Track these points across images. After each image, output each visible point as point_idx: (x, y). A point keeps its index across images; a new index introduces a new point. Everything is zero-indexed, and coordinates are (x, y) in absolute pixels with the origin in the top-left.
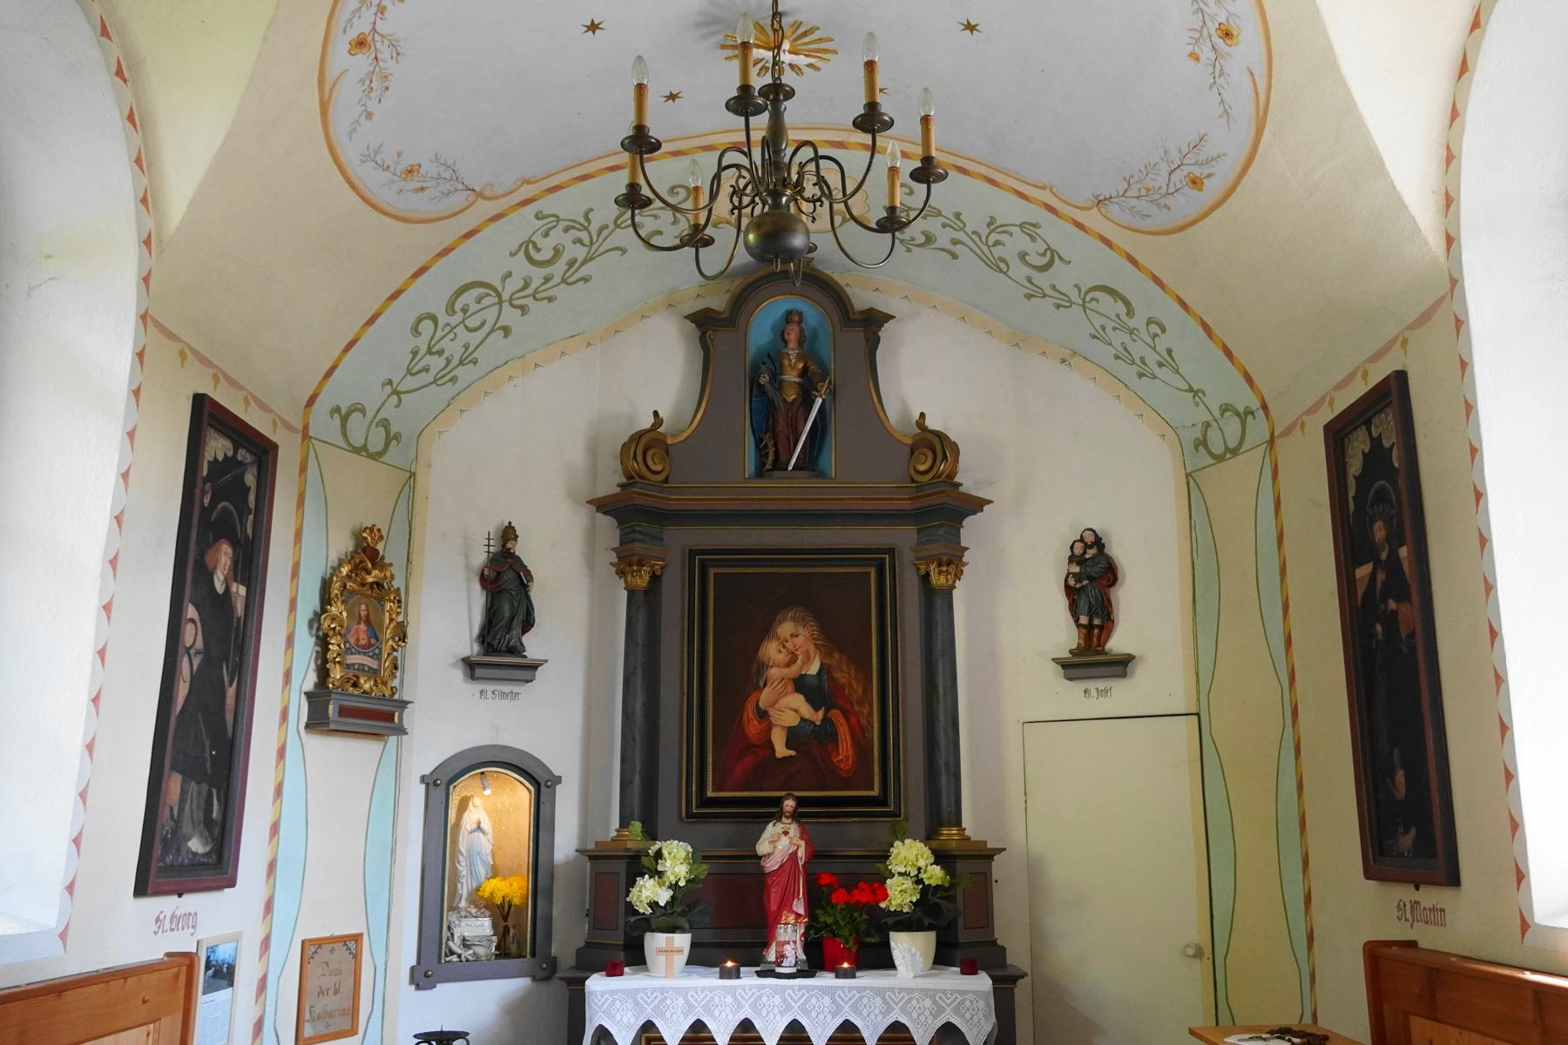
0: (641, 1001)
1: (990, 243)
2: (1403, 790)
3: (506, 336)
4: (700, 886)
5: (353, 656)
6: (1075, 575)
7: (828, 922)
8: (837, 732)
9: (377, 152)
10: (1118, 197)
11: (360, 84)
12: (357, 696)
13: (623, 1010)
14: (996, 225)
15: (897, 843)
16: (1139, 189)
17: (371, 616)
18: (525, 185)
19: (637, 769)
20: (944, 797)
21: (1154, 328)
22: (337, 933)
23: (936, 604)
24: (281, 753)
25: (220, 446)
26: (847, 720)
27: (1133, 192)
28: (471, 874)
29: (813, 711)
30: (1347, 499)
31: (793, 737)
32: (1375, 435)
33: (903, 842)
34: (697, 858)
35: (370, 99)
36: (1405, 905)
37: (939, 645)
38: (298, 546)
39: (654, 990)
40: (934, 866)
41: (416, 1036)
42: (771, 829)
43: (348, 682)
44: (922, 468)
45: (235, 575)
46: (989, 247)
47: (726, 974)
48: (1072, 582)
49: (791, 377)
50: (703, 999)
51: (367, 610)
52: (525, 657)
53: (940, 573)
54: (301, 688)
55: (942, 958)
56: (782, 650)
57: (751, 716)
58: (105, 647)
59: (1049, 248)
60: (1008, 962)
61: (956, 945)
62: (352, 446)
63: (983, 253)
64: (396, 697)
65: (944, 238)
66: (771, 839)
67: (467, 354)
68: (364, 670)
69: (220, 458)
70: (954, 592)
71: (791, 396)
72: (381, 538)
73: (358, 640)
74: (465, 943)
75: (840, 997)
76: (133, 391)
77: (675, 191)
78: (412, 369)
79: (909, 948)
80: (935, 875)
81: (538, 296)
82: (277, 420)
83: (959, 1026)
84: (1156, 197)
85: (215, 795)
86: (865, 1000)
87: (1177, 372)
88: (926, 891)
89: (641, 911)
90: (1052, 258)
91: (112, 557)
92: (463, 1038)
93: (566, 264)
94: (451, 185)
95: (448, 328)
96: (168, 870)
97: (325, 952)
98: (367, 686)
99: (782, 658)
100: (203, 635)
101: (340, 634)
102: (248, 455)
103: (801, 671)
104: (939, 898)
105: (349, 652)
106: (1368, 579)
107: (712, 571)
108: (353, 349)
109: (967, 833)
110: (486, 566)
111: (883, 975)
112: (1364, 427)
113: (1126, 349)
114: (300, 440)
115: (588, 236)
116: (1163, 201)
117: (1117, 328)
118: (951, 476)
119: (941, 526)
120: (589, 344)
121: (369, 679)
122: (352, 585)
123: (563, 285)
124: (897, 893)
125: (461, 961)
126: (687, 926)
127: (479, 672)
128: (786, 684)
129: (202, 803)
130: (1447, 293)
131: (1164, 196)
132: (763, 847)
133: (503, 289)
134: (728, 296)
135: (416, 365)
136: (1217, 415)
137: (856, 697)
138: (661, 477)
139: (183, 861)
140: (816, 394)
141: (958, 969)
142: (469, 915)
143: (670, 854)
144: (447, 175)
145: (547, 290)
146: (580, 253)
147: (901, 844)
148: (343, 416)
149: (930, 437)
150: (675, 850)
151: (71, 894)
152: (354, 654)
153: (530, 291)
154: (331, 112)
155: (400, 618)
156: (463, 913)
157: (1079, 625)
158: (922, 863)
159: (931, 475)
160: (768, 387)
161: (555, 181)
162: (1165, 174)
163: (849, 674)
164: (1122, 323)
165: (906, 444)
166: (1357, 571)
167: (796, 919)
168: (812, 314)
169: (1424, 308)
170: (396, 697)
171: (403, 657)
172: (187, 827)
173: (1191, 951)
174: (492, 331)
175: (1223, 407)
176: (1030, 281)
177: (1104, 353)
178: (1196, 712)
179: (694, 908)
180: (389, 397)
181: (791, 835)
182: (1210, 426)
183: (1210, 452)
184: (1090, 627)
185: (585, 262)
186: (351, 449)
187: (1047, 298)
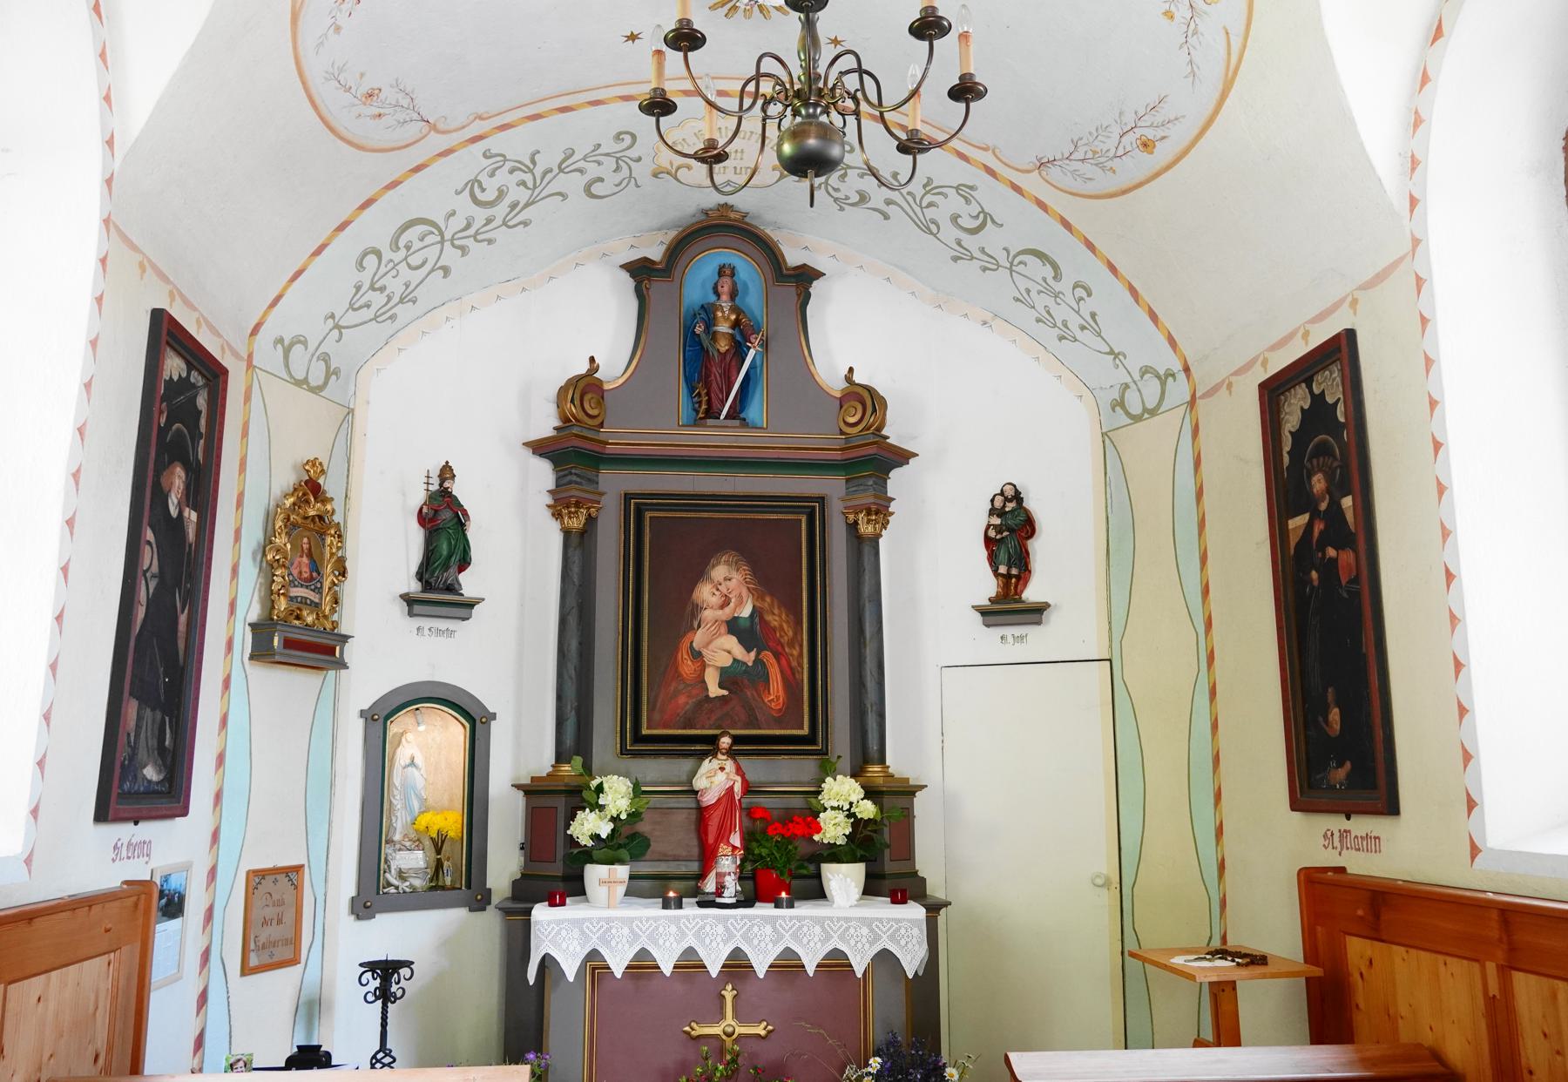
1: (924, 205)
2: (1337, 727)
3: (445, 277)
5: (295, 589)
7: (764, 854)
9: (341, 70)
12: (299, 628)
14: (932, 186)
16: (1086, 152)
17: (313, 549)
21: (1080, 292)
22: (280, 864)
23: (864, 550)
25: (175, 365)
27: (1079, 155)
30: (1282, 455)
31: (727, 678)
32: (1316, 391)
35: (340, 11)
36: (1332, 835)
37: (867, 589)
40: (865, 801)
41: (361, 965)
42: (708, 765)
44: (852, 420)
45: (188, 500)
46: (922, 208)
48: (992, 533)
49: (723, 328)
51: (310, 544)
52: (462, 595)
53: (869, 522)
55: (872, 888)
57: (685, 656)
58: (67, 563)
59: (983, 211)
62: (295, 379)
63: (915, 213)
64: (336, 631)
67: (407, 292)
68: (306, 603)
69: (175, 378)
70: (881, 540)
71: (723, 346)
72: (323, 471)
73: (300, 573)
74: (401, 875)
75: (781, 926)
76: (96, 298)
79: (844, 879)
80: (867, 810)
81: (479, 237)
85: (167, 723)
87: (1099, 335)
88: (858, 823)
89: (583, 843)
90: (985, 219)
91: (74, 470)
92: (409, 967)
93: (509, 207)
94: (407, 114)
95: (391, 265)
96: (125, 796)
97: (268, 883)
98: (310, 619)
99: (715, 600)
100: (159, 560)
101: (284, 566)
102: (200, 378)
104: (869, 831)
105: (292, 585)
106: (1302, 531)
107: (648, 515)
108: (299, 279)
109: (890, 770)
110: (425, 504)
111: (821, 905)
112: (1304, 385)
113: (1048, 312)
115: (531, 177)
116: (1109, 164)
121: (312, 612)
122: (295, 517)
126: (628, 858)
127: (417, 608)
128: (719, 626)
129: (156, 732)
130: (1407, 254)
131: (1111, 159)
133: (446, 228)
134: (664, 247)
135: (358, 300)
136: (1137, 377)
137: (786, 638)
138: (597, 422)
139: (139, 789)
140: (750, 345)
141: (889, 899)
144: (405, 102)
145: (487, 232)
146: (523, 195)
148: (286, 347)
149: (860, 390)
151: (35, 818)
152: (297, 586)
153: (471, 231)
154: (300, 23)
155: (340, 555)
156: (398, 846)
157: (996, 573)
158: (854, 798)
159: (860, 427)
160: (703, 336)
161: (507, 118)
163: (780, 617)
164: (1048, 287)
165: (835, 397)
166: (1290, 522)
167: (733, 851)
168: (748, 270)
169: (1379, 269)
170: (336, 631)
172: (142, 754)
173: (1099, 881)
174: (433, 270)
175: (1143, 370)
176: (959, 243)
177: (1026, 316)
180: (331, 330)
182: (1129, 388)
183: (1128, 413)
185: (527, 205)
186: (292, 381)
187: (975, 260)
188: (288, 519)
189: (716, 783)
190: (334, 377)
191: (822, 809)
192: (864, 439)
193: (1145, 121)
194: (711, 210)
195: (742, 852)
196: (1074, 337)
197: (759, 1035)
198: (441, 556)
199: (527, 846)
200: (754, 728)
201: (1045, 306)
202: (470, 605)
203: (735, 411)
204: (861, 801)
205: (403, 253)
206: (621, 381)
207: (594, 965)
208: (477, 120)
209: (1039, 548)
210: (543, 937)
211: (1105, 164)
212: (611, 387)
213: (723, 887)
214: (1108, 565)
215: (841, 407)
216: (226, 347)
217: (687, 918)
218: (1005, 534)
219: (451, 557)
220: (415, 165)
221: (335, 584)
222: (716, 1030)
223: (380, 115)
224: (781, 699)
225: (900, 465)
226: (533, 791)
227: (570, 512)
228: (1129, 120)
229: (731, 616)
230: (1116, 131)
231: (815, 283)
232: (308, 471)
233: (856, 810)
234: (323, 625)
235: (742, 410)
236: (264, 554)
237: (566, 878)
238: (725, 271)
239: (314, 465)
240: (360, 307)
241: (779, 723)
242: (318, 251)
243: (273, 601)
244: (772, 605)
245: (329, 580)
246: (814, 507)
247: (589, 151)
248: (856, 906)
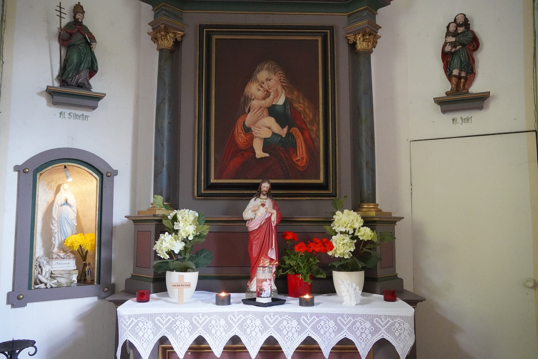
4: (204, 240)
6: (451, 43)
8: (296, 142)
15: (338, 213)
19: (165, 164)
20: (365, 184)
26: (303, 134)
28: (61, 231)
29: (280, 128)
31: (267, 145)
33: (342, 212)
34: (199, 221)
39: (167, 315)
40: (365, 228)
42: (254, 203)
47: (220, 302)
52: (91, 91)
57: (240, 131)
61: (375, 280)
66: (253, 209)
70: (372, 55)
74: (52, 276)
80: (366, 233)
83: (391, 341)
86: (322, 323)
88: (360, 244)
89: (162, 257)
92: (33, 346)
99: (260, 94)
103: (273, 103)
107: (214, 37)
109: (379, 207)
124: (340, 245)
125: (47, 288)
127: (57, 98)
128: (263, 111)
132: (247, 214)
137: (308, 119)
141: (382, 296)
142: (59, 257)
147: (341, 213)
150: (186, 216)
157: (449, 76)
158: (357, 225)
163: (304, 104)
167: (270, 262)
173: (531, 284)
178: (535, 130)
181: (267, 206)
191: (334, 233)
198: (72, 63)
200: (286, 179)
202: (98, 98)
210: (125, 328)
213: (262, 290)
218: (458, 47)
219: (81, 64)
224: (305, 159)
229: (271, 104)
233: (358, 234)
246: (327, 32)
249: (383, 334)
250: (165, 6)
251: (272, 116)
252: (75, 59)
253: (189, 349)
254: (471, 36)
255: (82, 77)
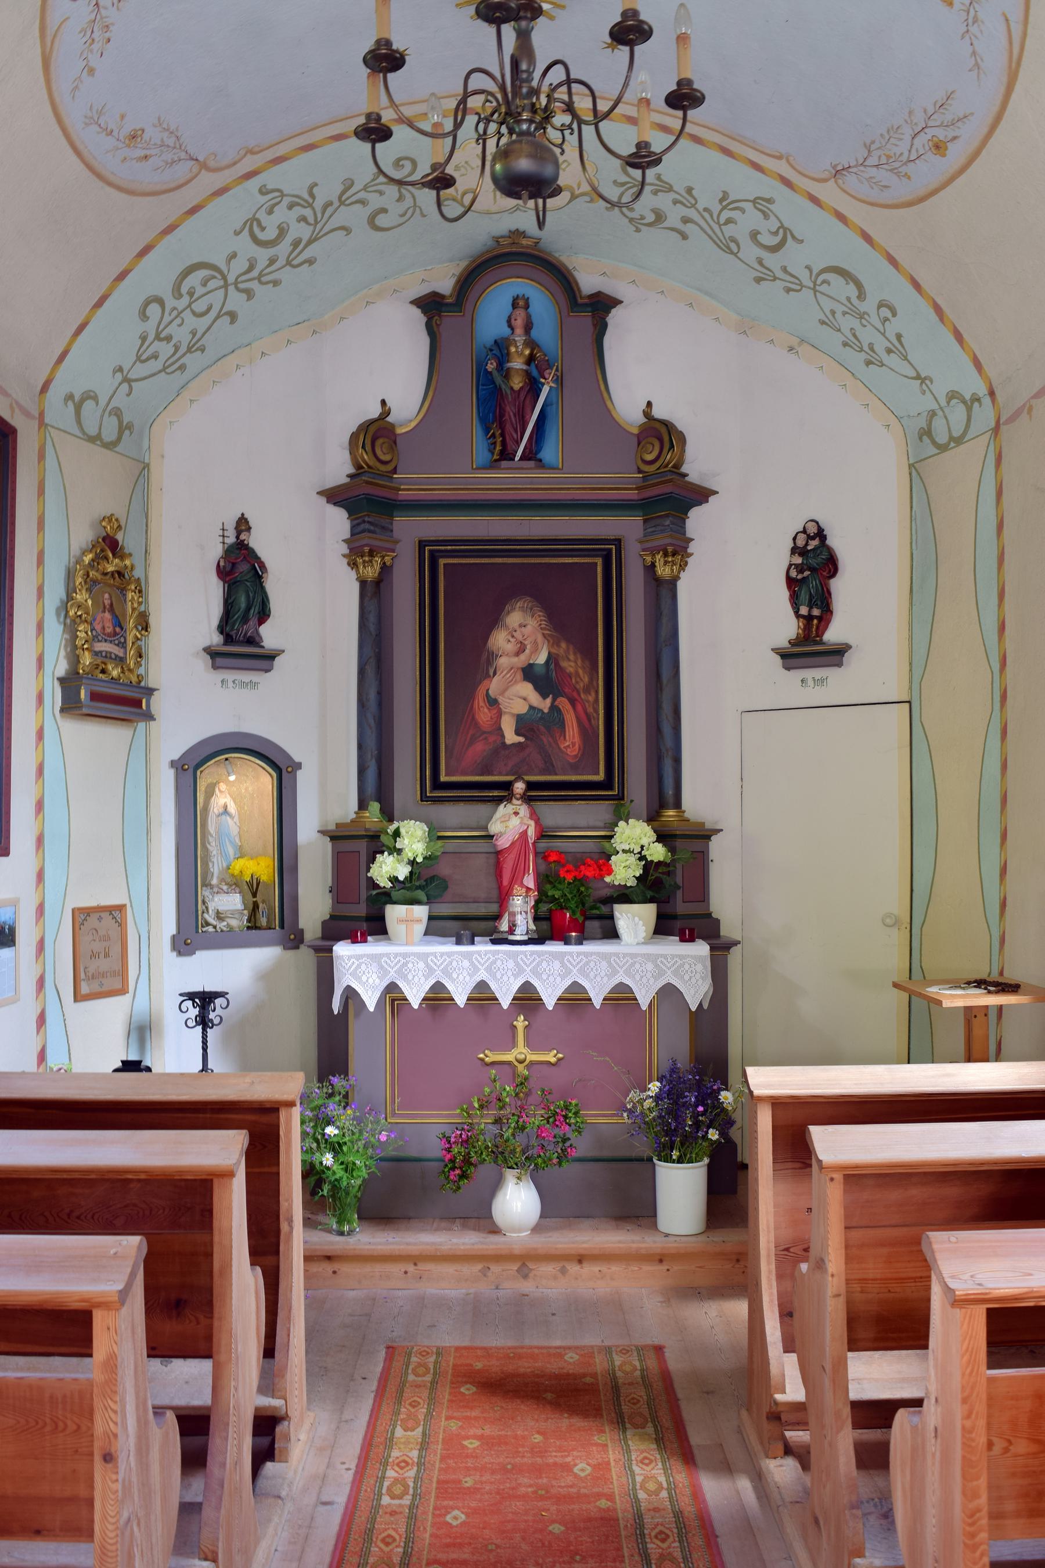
0: (385, 965)
3: (232, 322)
5: (99, 644)
6: (797, 566)
7: (556, 896)
9: (100, 113)
10: (856, 166)
11: (82, 34)
13: (369, 973)
16: (880, 157)
18: (249, 156)
21: (885, 312)
24: (40, 735)
26: (573, 705)
27: (873, 161)
29: (541, 699)
31: (523, 725)
33: (627, 822)
34: (435, 835)
35: (91, 51)
37: (664, 633)
38: (41, 534)
39: (396, 955)
41: (181, 995)
42: (503, 810)
43: (97, 668)
44: (649, 457)
46: (720, 226)
48: (793, 574)
49: (517, 364)
50: (442, 964)
53: (666, 563)
54: (53, 673)
55: (663, 927)
56: (511, 639)
57: (482, 704)
59: (782, 226)
60: (721, 934)
62: (87, 435)
64: (143, 684)
65: (674, 216)
68: (111, 658)
71: (517, 383)
72: (119, 527)
73: (104, 628)
74: (219, 916)
75: (569, 961)
77: (401, 163)
78: (141, 355)
80: (658, 852)
81: (263, 279)
82: (14, 405)
84: (897, 165)
86: (592, 964)
87: (906, 359)
88: (649, 866)
89: (382, 885)
90: (785, 235)
92: (223, 996)
94: (174, 154)
95: (175, 313)
97: (93, 921)
98: (115, 673)
99: (510, 647)
101: (86, 621)
105: (96, 640)
107: (442, 562)
110: (222, 557)
113: (854, 335)
114: (36, 427)
116: (903, 169)
117: (847, 313)
118: (678, 466)
119: (667, 516)
120: (315, 332)
121: (116, 666)
123: (288, 267)
124: (621, 868)
127: (220, 661)
128: (515, 673)
131: (905, 164)
135: (145, 351)
136: (943, 403)
137: (582, 685)
138: (390, 467)
140: (543, 381)
143: (407, 833)
144: (171, 141)
146: (304, 232)
148: (78, 403)
149: (657, 425)
153: (255, 273)
154: (52, 68)
155: (142, 608)
157: (798, 615)
158: (645, 841)
160: (495, 374)
162: (907, 138)
163: (576, 662)
167: (527, 892)
171: (147, 645)
175: (950, 395)
176: (760, 262)
179: (431, 884)
183: (934, 443)
184: (809, 618)
187: (777, 281)
188: (88, 576)
189: (511, 827)
190: (127, 432)
192: (661, 477)
193: (935, 120)
194: (502, 237)
195: (536, 893)
196: (881, 362)
197: (549, 1063)
199: (335, 890)
200: (550, 774)
201: (851, 329)
202: (269, 658)
203: (531, 452)
204: (651, 844)
205: (185, 300)
206: (413, 424)
207: (393, 996)
208: (248, 155)
209: (841, 588)
211: (900, 170)
212: (404, 431)
213: (515, 925)
214: (911, 604)
215: (639, 444)
216: (14, 405)
217: (479, 953)
218: (807, 573)
220: (190, 206)
221: (138, 639)
222: (509, 1057)
223: (146, 157)
225: (699, 503)
226: (338, 836)
227: (364, 562)
228: (919, 119)
230: (908, 132)
231: (614, 311)
232: (105, 527)
234: (128, 678)
235: (539, 450)
236: (67, 612)
237: (369, 919)
238: (519, 303)
239: (110, 521)
240: (148, 359)
241: (575, 768)
242: (99, 303)
243: (78, 656)
244: (567, 651)
245: (132, 634)
246: (610, 550)
247: (369, 180)
248: (643, 943)
249: (669, 978)
250: (368, 515)
251: (529, 682)
252: (243, 602)
253: (423, 1000)
254: (825, 556)
255: (249, 628)
